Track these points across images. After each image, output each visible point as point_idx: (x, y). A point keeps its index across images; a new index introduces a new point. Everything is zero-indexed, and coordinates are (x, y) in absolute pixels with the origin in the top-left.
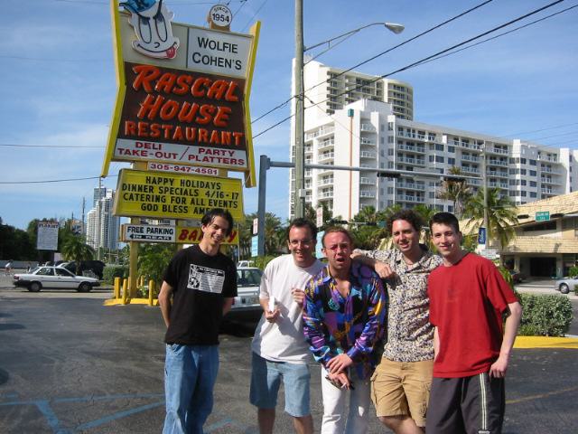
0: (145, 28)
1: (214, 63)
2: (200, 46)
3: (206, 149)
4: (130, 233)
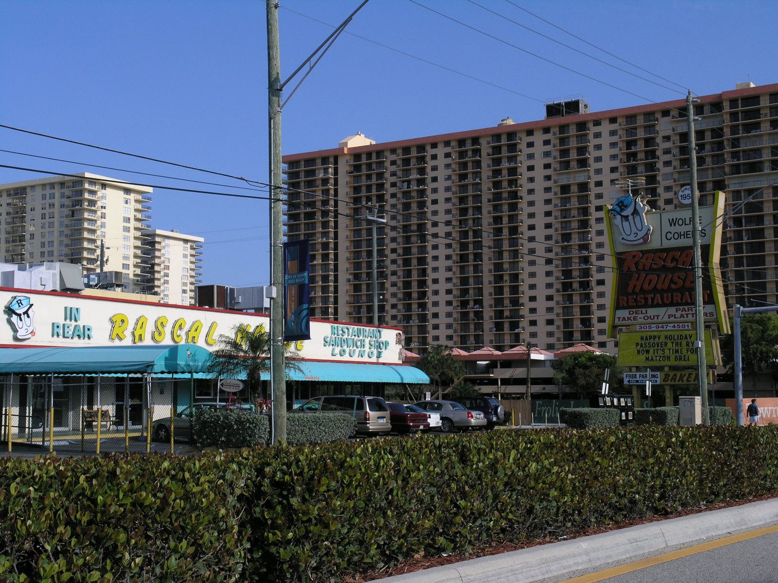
0: (626, 224)
1: (682, 237)
2: (671, 225)
3: (681, 308)
4: (628, 379)
